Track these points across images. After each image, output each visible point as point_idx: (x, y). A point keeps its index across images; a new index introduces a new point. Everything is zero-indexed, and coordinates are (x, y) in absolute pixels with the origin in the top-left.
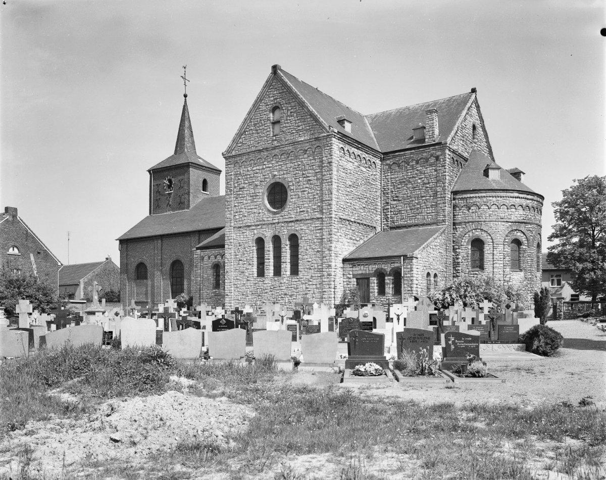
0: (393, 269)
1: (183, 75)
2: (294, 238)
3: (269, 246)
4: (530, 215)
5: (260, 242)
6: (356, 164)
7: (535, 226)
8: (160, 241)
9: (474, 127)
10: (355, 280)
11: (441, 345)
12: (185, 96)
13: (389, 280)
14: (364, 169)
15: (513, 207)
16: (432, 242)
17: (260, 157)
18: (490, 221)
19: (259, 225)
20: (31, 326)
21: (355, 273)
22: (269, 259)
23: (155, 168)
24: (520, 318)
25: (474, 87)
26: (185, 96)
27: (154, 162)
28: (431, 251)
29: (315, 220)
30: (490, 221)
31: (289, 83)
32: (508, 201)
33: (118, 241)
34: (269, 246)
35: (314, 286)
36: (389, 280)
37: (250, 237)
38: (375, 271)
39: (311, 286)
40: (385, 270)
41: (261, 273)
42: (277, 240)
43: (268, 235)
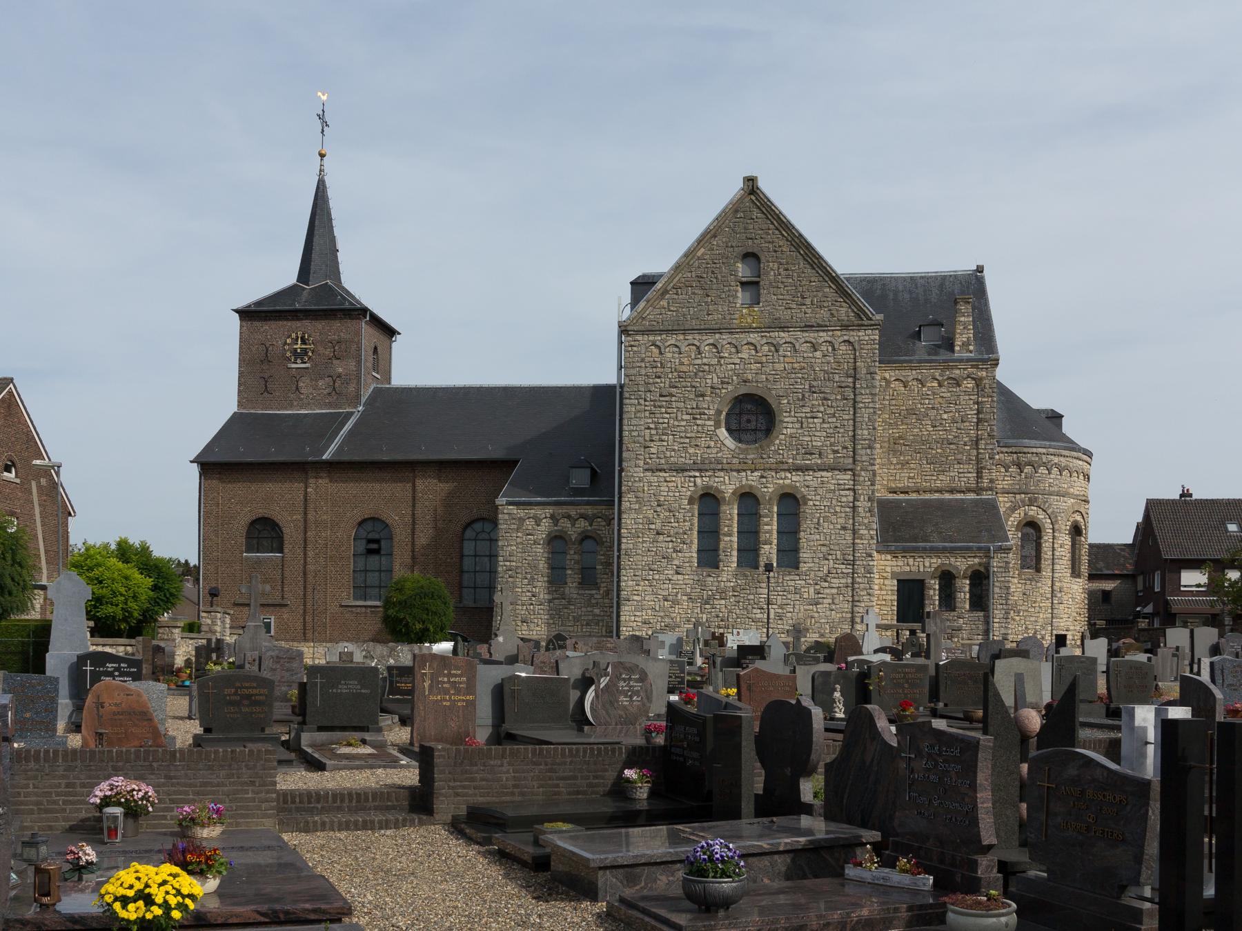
0: (970, 566)
2: (790, 502)
3: (731, 514)
5: (709, 501)
10: (895, 582)
12: (322, 156)
18: (305, 574)
20: (1176, 679)
21: (895, 569)
22: (730, 535)
23: (253, 308)
26: (322, 156)
27: (251, 295)
30: (305, 574)
34: (731, 514)
35: (834, 591)
37: (681, 489)
38: (936, 569)
39: (827, 591)
40: (956, 568)
41: (709, 557)
42: (748, 498)
43: (728, 485)
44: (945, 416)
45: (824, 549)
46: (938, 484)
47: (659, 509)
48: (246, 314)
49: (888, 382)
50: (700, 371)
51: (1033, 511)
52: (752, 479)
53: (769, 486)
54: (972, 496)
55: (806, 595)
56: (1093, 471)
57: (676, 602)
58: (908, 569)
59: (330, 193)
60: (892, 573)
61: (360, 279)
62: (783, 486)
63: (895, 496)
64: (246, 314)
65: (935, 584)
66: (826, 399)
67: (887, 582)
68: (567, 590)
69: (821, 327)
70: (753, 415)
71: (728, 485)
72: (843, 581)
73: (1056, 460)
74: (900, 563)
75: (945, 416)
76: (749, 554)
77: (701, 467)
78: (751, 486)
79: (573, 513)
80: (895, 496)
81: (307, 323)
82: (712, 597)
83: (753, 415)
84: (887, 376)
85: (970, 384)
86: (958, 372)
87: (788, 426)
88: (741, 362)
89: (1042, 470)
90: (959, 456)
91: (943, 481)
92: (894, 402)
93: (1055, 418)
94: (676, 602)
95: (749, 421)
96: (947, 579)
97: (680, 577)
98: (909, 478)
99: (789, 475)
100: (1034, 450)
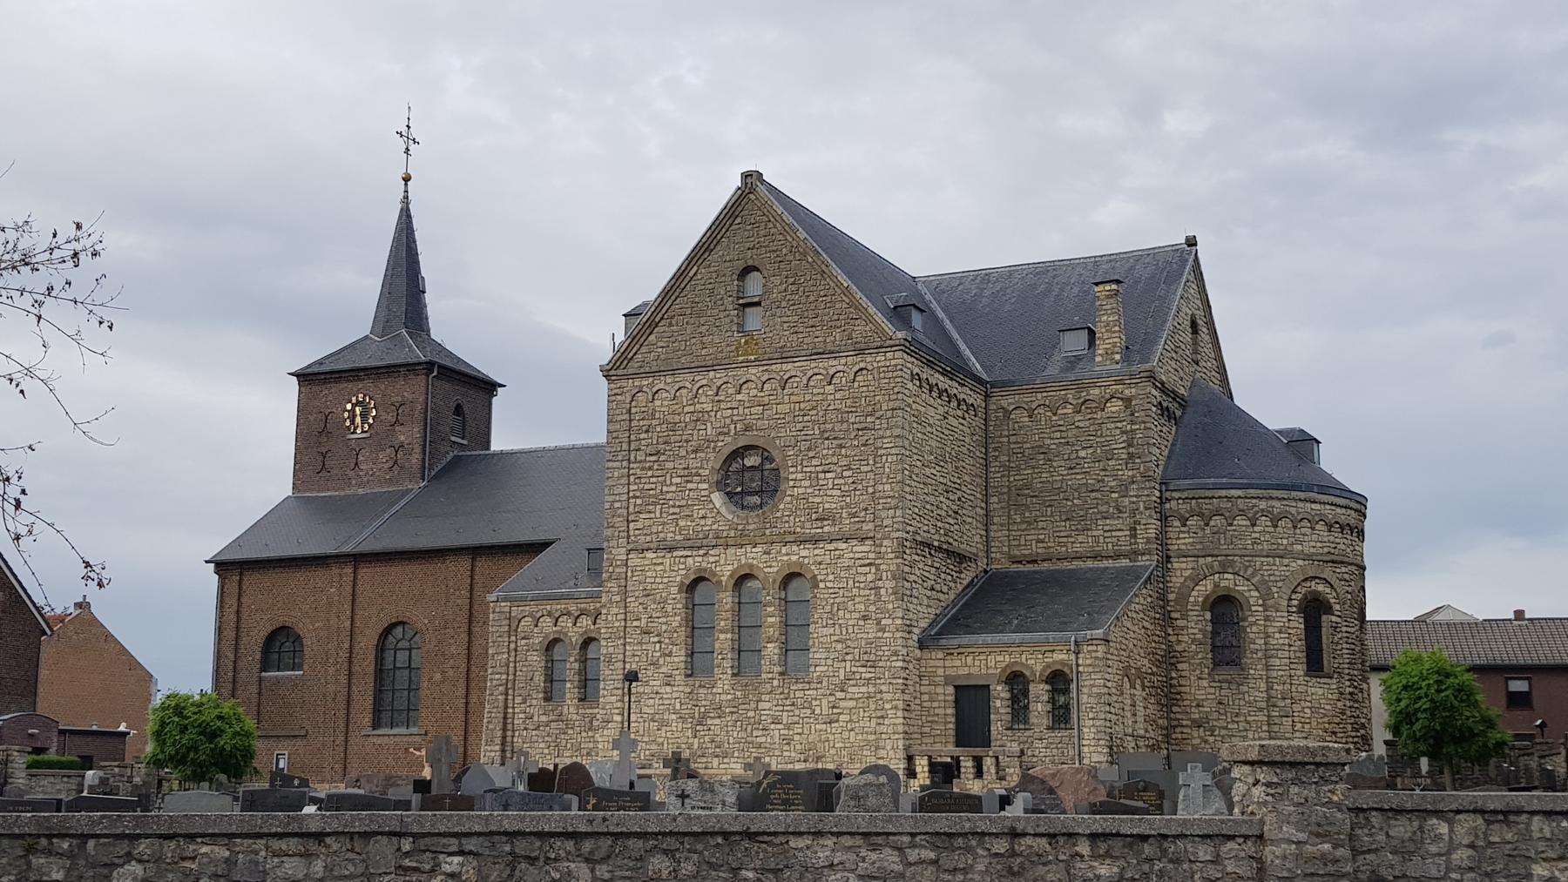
0: (1048, 666)
1: (404, 130)
4: (1342, 542)
6: (941, 410)
7: (1353, 568)
8: (349, 570)
9: (1194, 325)
10: (951, 690)
11: (83, 605)
12: (407, 179)
13: (1039, 692)
14: (955, 422)
15: (1305, 523)
16: (1130, 602)
17: (704, 382)
19: (699, 548)
21: (949, 672)
24: (488, 442)
25: (1191, 234)
26: (407, 179)
28: (1129, 625)
29: (854, 542)
31: (963, 346)
32: (1293, 510)
33: (212, 565)
36: (1039, 692)
38: (1004, 670)
44: (1082, 454)
45: (839, 646)
46: (1078, 548)
47: (645, 600)
48: (304, 377)
49: (1007, 413)
50: (699, 419)
51: (1228, 581)
52: (752, 556)
53: (769, 563)
54: (1125, 562)
55: (818, 711)
56: (1368, 512)
57: (664, 724)
58: (965, 671)
59: (416, 224)
60: (946, 677)
61: (455, 325)
62: (790, 564)
63: (1021, 568)
64: (304, 377)
65: (1000, 692)
66: (841, 447)
67: (940, 690)
68: (565, 711)
69: (832, 354)
70: (749, 477)
71: (725, 565)
72: (864, 689)
73: (1263, 505)
74: (958, 663)
75: (1082, 454)
76: (745, 655)
77: (694, 544)
78: (751, 566)
79: (572, 608)
80: (1021, 568)
81: (368, 383)
82: (704, 716)
83: (749, 477)
84: (1004, 403)
85: (1115, 407)
86: (1097, 391)
87: (796, 483)
88: (727, 403)
89: (1241, 521)
90: (1103, 508)
91: (1081, 544)
92: (1013, 439)
93: (1302, 444)
94: (664, 724)
95: (752, 480)
96: (1016, 680)
97: (668, 689)
98: (1039, 541)
99: (795, 548)
100: (1223, 493)
